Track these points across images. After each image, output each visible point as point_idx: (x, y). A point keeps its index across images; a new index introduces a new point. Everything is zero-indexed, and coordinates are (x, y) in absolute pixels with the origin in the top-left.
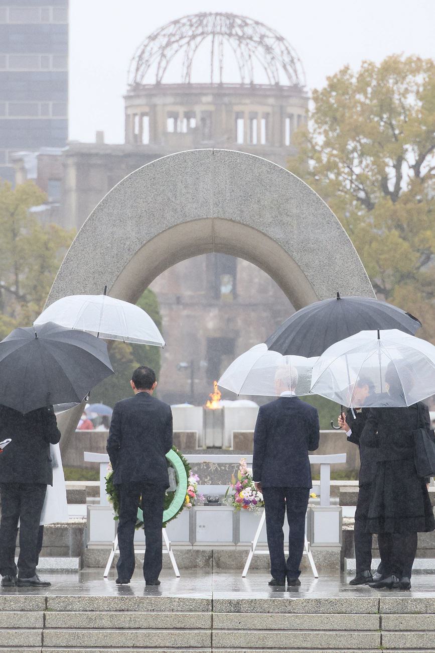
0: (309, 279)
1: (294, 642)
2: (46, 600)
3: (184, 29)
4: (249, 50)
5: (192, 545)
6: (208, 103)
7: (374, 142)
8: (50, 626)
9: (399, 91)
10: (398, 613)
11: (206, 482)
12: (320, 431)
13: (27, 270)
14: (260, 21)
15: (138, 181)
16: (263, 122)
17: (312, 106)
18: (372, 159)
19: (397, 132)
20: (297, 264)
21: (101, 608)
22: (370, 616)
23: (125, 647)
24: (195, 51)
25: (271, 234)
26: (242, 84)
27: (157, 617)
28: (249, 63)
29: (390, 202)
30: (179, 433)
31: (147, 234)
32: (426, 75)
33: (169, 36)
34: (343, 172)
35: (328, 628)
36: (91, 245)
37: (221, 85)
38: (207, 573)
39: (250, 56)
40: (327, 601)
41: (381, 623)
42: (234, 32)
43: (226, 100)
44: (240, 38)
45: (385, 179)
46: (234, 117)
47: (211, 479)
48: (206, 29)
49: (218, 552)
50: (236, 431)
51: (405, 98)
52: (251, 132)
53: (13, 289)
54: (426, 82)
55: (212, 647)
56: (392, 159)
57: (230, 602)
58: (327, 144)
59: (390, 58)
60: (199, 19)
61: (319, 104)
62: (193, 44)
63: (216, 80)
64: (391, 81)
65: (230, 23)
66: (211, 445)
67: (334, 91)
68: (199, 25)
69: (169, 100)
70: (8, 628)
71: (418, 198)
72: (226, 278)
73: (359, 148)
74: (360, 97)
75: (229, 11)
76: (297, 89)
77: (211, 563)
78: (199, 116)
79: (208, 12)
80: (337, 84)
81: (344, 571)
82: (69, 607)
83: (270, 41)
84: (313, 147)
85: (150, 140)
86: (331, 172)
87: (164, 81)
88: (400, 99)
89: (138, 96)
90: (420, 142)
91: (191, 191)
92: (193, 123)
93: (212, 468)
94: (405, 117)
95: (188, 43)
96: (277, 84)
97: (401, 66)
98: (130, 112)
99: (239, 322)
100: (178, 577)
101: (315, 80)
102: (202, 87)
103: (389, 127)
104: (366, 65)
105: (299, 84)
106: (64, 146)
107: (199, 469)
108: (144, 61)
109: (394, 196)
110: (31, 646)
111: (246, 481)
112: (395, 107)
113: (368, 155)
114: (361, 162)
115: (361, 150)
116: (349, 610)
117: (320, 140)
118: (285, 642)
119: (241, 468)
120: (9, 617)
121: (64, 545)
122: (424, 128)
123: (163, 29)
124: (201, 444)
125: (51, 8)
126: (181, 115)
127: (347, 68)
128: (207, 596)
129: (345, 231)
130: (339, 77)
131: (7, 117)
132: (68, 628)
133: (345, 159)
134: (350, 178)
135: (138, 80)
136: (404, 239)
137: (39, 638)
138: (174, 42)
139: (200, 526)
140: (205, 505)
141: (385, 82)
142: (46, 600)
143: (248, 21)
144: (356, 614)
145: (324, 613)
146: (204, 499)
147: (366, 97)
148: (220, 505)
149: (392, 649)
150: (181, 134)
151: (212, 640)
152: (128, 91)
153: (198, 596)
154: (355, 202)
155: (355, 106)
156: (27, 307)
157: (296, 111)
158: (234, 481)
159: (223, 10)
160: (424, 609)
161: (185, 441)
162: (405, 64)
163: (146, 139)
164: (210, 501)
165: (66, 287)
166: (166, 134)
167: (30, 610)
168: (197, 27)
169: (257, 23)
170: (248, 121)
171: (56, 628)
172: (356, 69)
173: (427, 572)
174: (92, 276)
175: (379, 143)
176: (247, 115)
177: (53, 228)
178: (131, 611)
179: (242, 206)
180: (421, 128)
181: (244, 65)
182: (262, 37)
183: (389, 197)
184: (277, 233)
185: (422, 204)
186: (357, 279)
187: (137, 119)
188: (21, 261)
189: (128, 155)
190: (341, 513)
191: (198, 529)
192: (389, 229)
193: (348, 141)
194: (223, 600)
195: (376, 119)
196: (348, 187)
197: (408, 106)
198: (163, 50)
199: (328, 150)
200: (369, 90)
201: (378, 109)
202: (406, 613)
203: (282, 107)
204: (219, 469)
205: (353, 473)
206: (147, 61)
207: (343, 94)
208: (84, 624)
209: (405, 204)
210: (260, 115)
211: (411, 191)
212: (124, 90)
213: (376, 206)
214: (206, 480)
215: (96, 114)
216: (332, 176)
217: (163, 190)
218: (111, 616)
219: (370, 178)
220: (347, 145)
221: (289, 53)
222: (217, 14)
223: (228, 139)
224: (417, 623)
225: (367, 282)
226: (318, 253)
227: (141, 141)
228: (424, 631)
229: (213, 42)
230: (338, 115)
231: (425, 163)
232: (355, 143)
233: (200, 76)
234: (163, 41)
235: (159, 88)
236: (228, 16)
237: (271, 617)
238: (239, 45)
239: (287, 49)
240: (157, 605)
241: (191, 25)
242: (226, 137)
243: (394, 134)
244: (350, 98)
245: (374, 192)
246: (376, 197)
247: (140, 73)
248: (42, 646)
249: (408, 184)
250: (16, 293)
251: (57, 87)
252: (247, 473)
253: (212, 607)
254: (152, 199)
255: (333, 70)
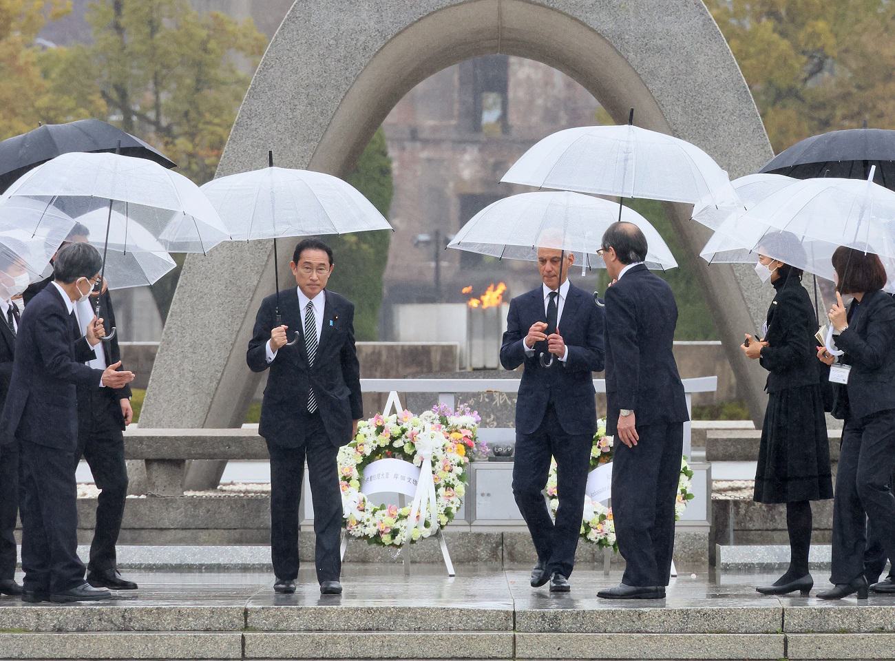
0: (655, 95)
2: (246, 612)
5: (470, 526)
8: (253, 656)
10: (813, 632)
12: (675, 343)
20: (635, 71)
21: (335, 626)
22: (769, 637)
31: (393, 23)
36: (304, 42)
38: (494, 571)
40: (699, 612)
47: (497, 419)
53: (151, 115)
66: (480, 365)
72: (491, 98)
77: (500, 554)
81: (715, 565)
82: (283, 625)
93: (498, 401)
100: (451, 576)
107: (478, 403)
116: (734, 627)
120: (185, 641)
124: (464, 365)
129: (713, 19)
136: (783, 34)
139: (482, 495)
140: (491, 459)
142: (246, 612)
144: (746, 633)
145: (694, 633)
146: (488, 450)
156: (175, 145)
161: (438, 358)
164: (498, 454)
165: (263, 110)
167: (220, 630)
174: (304, 91)
177: (216, 17)
178: (384, 630)
186: (732, 95)
188: (164, 72)
190: (709, 472)
191: (479, 499)
202: (827, 632)
204: (510, 403)
205: (706, 411)
214: (488, 421)
218: (352, 639)
224: (845, 648)
225: (748, 101)
226: (669, 54)
237: (610, 639)
240: (425, 621)
250: (157, 123)
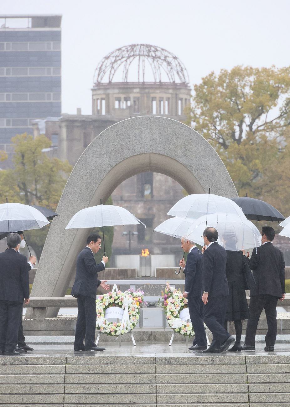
1: (200, 380)
2: (66, 358)
3: (123, 53)
4: (159, 64)
6: (138, 93)
7: (227, 113)
9: (241, 85)
10: (256, 364)
11: (147, 295)
13: (42, 183)
14: (164, 48)
15: (109, 133)
16: (166, 102)
17: (193, 93)
18: (227, 121)
19: (240, 107)
23: (109, 383)
24: (129, 65)
25: (181, 162)
26: (139, 82)
27: (126, 367)
28: (159, 71)
29: (237, 145)
30: (127, 269)
32: (255, 77)
33: (115, 57)
34: (211, 129)
35: (218, 372)
37: (144, 83)
39: (159, 67)
41: (247, 369)
42: (150, 55)
43: (147, 91)
44: (154, 58)
45: (234, 133)
46: (151, 99)
47: (150, 293)
48: (135, 53)
49: (155, 332)
50: (158, 268)
51: (244, 89)
52: (160, 108)
53: (34, 193)
54: (255, 80)
55: (156, 383)
56: (237, 121)
57: (165, 359)
58: (202, 114)
59: (236, 67)
60: (132, 48)
61: (198, 93)
62: (128, 61)
63: (141, 80)
64: (236, 80)
65: (148, 50)
66: (144, 276)
67: (206, 85)
68: (133, 51)
69: (116, 91)
70: (46, 374)
71: (251, 142)
72: (147, 186)
73: (219, 115)
74: (220, 89)
75: (148, 43)
76: (184, 85)
77: (151, 338)
78: (132, 100)
79: (136, 44)
80: (207, 82)
83: (170, 59)
84: (195, 115)
85: (106, 112)
86: (205, 129)
87: (113, 81)
88: (241, 90)
89: (99, 89)
90: (252, 112)
91: (138, 138)
92: (129, 103)
93: (150, 287)
94: (244, 99)
95: (126, 61)
96: (174, 82)
97: (242, 72)
98: (95, 97)
99: (155, 210)
100: (135, 346)
101: (194, 79)
102: (133, 84)
103: (235, 104)
104: (223, 71)
105: (185, 82)
106: (59, 117)
107: (143, 288)
108: (102, 71)
109: (239, 141)
110: (58, 384)
111: (170, 294)
112: (239, 94)
113: (225, 119)
114: (220, 123)
115: (221, 117)
117: (199, 111)
118: (195, 380)
119: (166, 287)
121: (72, 329)
122: (254, 105)
123: (112, 53)
124: (139, 275)
125: (52, 43)
126: (122, 99)
127: (213, 73)
128: (152, 356)
130: (208, 77)
131: (29, 101)
132: (78, 374)
133: (212, 122)
134: (215, 132)
135: (99, 80)
136: (245, 164)
137: (63, 379)
138: (118, 60)
139: (145, 319)
140: (148, 307)
141: (233, 80)
143: (158, 49)
146: (147, 304)
147: (223, 89)
148: (156, 307)
149: (253, 383)
150: (123, 109)
151: (156, 379)
152: (94, 86)
153: (148, 356)
154: (218, 145)
155: (217, 93)
156: (42, 202)
157: (184, 96)
158: (163, 294)
159: (145, 43)
160: (269, 362)
162: (244, 71)
163: (104, 113)
164: (150, 305)
166: (114, 109)
167: (58, 364)
168: (130, 52)
169: (163, 50)
170: (158, 102)
171: (72, 373)
172: (217, 74)
173: (285, 342)
175: (231, 113)
176: (158, 99)
179: (165, 147)
180: (253, 105)
181: (156, 72)
182: (166, 57)
183: (236, 142)
184: (185, 161)
185: (253, 146)
187: (99, 101)
188: (39, 178)
189: (95, 121)
191: (144, 320)
192: (236, 159)
193: (214, 112)
194: (162, 358)
195: (229, 100)
196: (214, 137)
197: (246, 93)
198: (113, 65)
199: (203, 117)
200: (225, 85)
201: (230, 95)
203: (176, 94)
206: (104, 70)
207: (211, 87)
208: (87, 372)
209: (245, 145)
210: (165, 99)
211: (248, 139)
212: (92, 85)
213: (229, 147)
215: (76, 99)
216: (205, 131)
217: (123, 138)
219: (226, 132)
220: (213, 114)
221: (180, 65)
222: (141, 45)
223: (148, 112)
227: (101, 113)
228: (270, 373)
229: (139, 60)
230: (208, 98)
231: (255, 124)
232: (217, 113)
233: (133, 78)
234: (113, 60)
235: (110, 84)
236: (147, 46)
238: (153, 62)
239: (179, 63)
241: (128, 51)
242: (147, 111)
243: (238, 108)
244: (214, 89)
245: (228, 139)
246: (229, 142)
247: (100, 77)
248: (65, 383)
249: (246, 135)
250: (36, 195)
251: (55, 85)
252: (170, 290)
253: (156, 362)
254: (117, 143)
255: (206, 74)
